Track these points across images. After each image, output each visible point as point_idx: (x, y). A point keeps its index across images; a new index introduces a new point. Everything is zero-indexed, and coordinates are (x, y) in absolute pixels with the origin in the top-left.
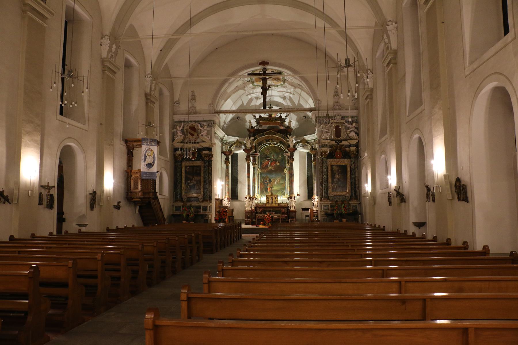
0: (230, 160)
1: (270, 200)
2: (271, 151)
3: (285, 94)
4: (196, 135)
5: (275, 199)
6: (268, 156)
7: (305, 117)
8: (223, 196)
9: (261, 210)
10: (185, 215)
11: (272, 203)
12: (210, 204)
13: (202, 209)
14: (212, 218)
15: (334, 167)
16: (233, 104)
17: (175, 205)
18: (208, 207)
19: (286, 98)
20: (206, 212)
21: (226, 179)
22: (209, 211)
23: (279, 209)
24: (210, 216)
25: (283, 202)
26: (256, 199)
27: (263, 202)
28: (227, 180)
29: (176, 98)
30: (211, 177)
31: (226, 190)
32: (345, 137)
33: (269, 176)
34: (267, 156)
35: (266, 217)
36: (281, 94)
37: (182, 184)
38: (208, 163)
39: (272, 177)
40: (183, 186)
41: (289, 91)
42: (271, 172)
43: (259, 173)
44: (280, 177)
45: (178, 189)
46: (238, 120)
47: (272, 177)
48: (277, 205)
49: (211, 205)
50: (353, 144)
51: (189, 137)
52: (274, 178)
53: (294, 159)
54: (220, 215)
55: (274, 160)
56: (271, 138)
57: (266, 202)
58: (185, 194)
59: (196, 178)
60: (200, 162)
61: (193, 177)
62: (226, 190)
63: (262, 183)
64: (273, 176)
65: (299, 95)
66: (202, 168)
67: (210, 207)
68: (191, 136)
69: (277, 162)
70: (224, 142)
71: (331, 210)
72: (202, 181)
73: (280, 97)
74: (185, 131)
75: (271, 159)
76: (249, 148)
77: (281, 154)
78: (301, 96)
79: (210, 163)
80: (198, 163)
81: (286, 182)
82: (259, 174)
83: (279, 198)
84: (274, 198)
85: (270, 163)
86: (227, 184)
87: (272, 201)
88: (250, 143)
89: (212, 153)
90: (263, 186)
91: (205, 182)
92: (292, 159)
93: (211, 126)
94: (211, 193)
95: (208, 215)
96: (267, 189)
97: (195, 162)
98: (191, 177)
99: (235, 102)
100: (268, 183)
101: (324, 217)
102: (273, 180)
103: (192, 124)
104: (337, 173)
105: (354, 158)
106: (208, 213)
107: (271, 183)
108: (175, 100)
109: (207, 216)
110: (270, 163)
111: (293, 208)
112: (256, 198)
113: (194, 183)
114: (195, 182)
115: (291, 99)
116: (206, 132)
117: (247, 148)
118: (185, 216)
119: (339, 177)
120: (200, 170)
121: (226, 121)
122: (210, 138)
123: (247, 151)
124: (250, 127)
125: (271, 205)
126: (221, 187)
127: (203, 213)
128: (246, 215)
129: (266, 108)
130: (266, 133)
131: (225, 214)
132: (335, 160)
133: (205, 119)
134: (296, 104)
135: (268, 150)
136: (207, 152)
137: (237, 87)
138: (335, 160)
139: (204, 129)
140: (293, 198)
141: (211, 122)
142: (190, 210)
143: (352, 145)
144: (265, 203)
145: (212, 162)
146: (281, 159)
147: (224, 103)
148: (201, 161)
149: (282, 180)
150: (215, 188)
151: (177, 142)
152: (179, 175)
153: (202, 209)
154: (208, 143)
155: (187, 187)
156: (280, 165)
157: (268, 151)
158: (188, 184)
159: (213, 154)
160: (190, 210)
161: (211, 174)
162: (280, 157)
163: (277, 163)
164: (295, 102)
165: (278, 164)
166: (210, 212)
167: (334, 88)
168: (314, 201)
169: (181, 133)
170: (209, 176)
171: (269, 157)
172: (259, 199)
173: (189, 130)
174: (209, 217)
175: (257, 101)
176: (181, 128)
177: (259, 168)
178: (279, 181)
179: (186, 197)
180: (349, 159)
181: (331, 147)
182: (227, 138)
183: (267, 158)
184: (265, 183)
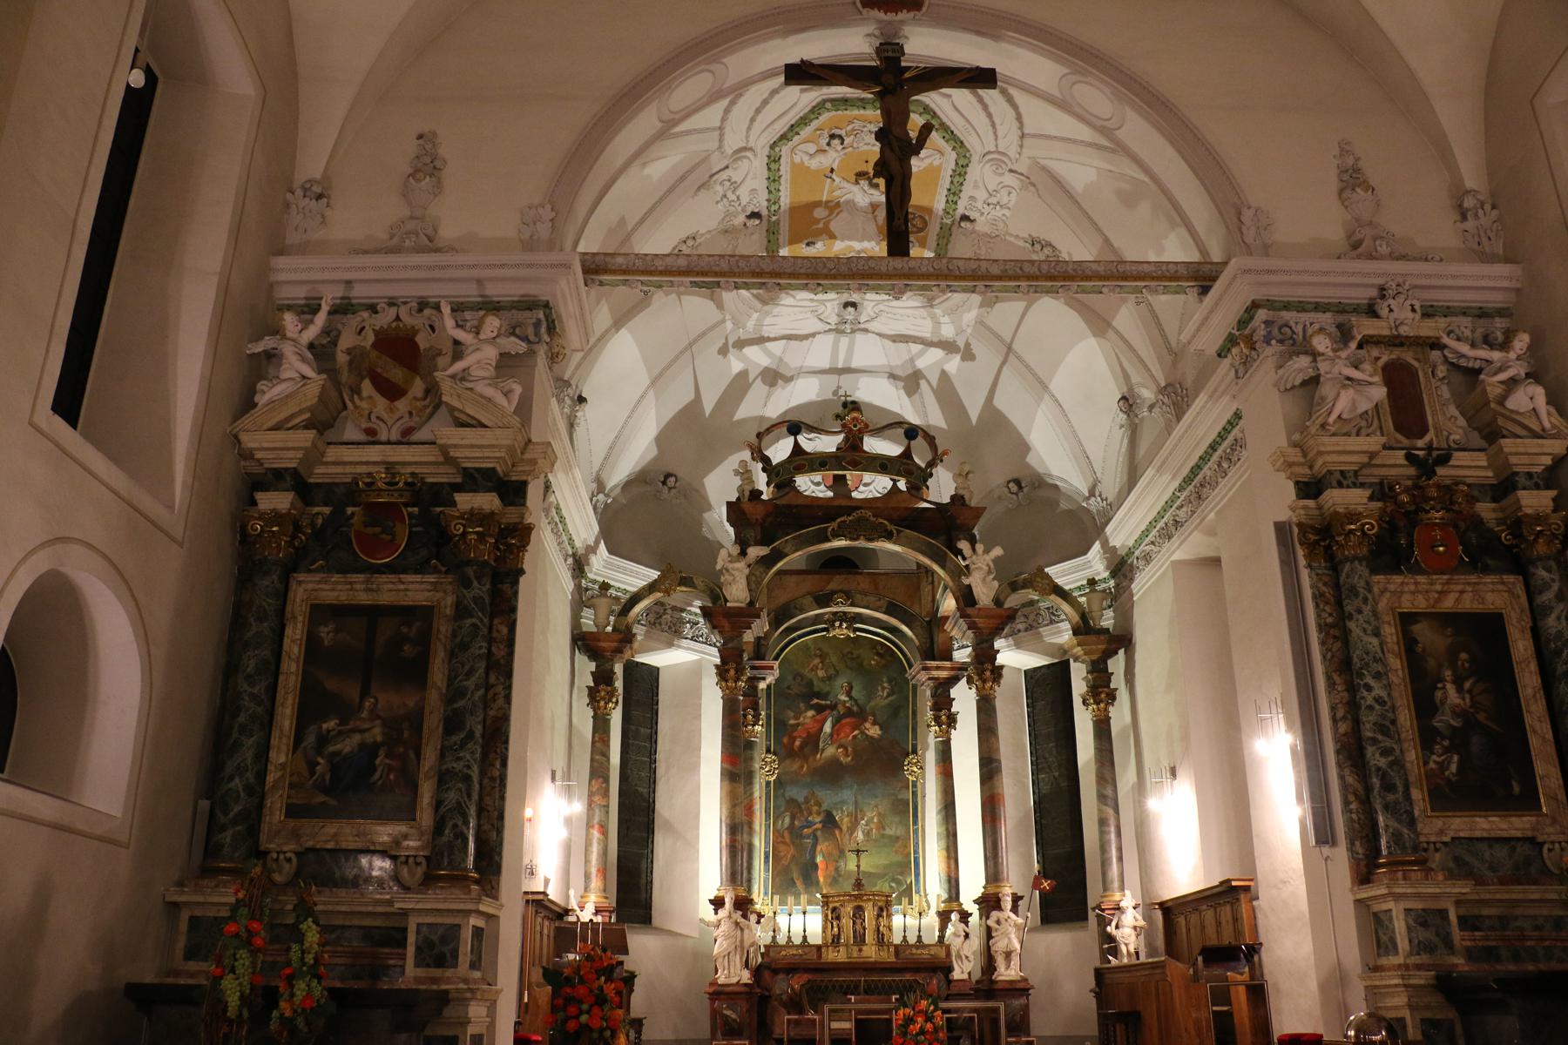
0: (619, 684)
1: (847, 922)
2: (834, 659)
3: (920, 354)
4: (420, 395)
5: (879, 916)
6: (818, 686)
7: (1017, 482)
8: (572, 893)
9: (798, 982)
10: (232, 992)
11: (860, 939)
12: (482, 908)
13: (411, 950)
14: (492, 1026)
15: (1421, 630)
16: (648, 382)
17: (186, 904)
18: (467, 935)
19: (923, 383)
20: (449, 973)
21: (591, 795)
22: (474, 965)
23: (908, 977)
24: (476, 1011)
25: (905, 937)
26: (758, 922)
27: (805, 937)
28: (596, 799)
29: (311, 166)
30: (508, 699)
31: (587, 861)
32: (1460, 431)
33: (827, 797)
34: (816, 689)
35: (909, 1020)
36: (898, 356)
37: (274, 742)
38: (494, 584)
39: (842, 800)
40: (279, 755)
41: (948, 331)
42: (832, 774)
43: (772, 779)
44: (884, 805)
45: (231, 779)
46: (665, 489)
47: (843, 802)
48: (887, 956)
49: (492, 918)
50: (1530, 475)
51: (364, 405)
52: (851, 808)
53: (1000, 676)
54: (569, 1000)
55: (849, 713)
56: (840, 588)
57: (824, 938)
58: (292, 823)
59: (387, 699)
60: (432, 578)
61: (365, 692)
62: (587, 861)
63: (786, 834)
64: (847, 795)
65: (1005, 349)
66: (443, 628)
67: (478, 932)
68: (378, 397)
69: (866, 720)
70: (587, 589)
71: (1468, 949)
72: (433, 721)
73: (893, 376)
74: (342, 358)
75: (833, 707)
76: (743, 605)
77: (890, 681)
78: (1012, 358)
79: (506, 587)
80: (415, 589)
81: (916, 832)
82: (768, 783)
83: (897, 921)
84: (869, 913)
85: (827, 728)
86: (596, 820)
87: (858, 927)
88: (748, 578)
89: (522, 516)
90: (792, 850)
91: (452, 724)
92: (988, 673)
93: (532, 338)
94: (501, 817)
95: (464, 1002)
96: (816, 866)
97: (392, 577)
98: (352, 692)
99: (661, 374)
100: (819, 833)
101: (1427, 1007)
102: (846, 820)
103: (398, 318)
104: (1448, 674)
105: (1552, 563)
106: (466, 981)
107: (837, 832)
108: (300, 177)
109: (447, 1012)
110: (827, 728)
111: (1008, 967)
112: (760, 916)
113: (368, 738)
114: (377, 734)
115: (946, 392)
116: (490, 353)
117: (728, 604)
118: (233, 1000)
119: (1467, 696)
120: (425, 639)
121: (604, 476)
122: (516, 397)
123: (725, 623)
124: (747, 494)
125: (855, 954)
126: (563, 834)
127: (417, 980)
128: (715, 1014)
129: (907, 254)
130: (834, 525)
131: (610, 989)
132: (1416, 583)
133: (496, 291)
134: (974, 414)
135: (816, 655)
136: (487, 501)
137: (690, 243)
138: (1416, 583)
139: (482, 336)
140: (1007, 903)
141: (530, 317)
142: (295, 947)
143: (1522, 480)
144: (819, 942)
145: (522, 580)
146: (889, 705)
147: (607, 331)
148: (436, 570)
149: (897, 819)
150: (527, 825)
151: (270, 424)
152: (251, 666)
153: (411, 950)
154: (498, 432)
155: (312, 766)
156: (881, 738)
157: (817, 661)
158: (323, 740)
159: (529, 520)
160: (295, 947)
161: (509, 675)
162: (883, 696)
163: (868, 725)
164: (966, 403)
165: (874, 731)
166: (477, 974)
167: (1336, 151)
168: (1114, 924)
169: (303, 359)
170: (488, 687)
171: (828, 693)
172: (782, 921)
173: (374, 354)
174: (465, 1023)
175: (768, 397)
176: (312, 332)
177: (768, 751)
178: (881, 826)
179: (290, 847)
180: (1509, 578)
181: (1383, 491)
182: (608, 565)
183: (815, 701)
184: (801, 836)
